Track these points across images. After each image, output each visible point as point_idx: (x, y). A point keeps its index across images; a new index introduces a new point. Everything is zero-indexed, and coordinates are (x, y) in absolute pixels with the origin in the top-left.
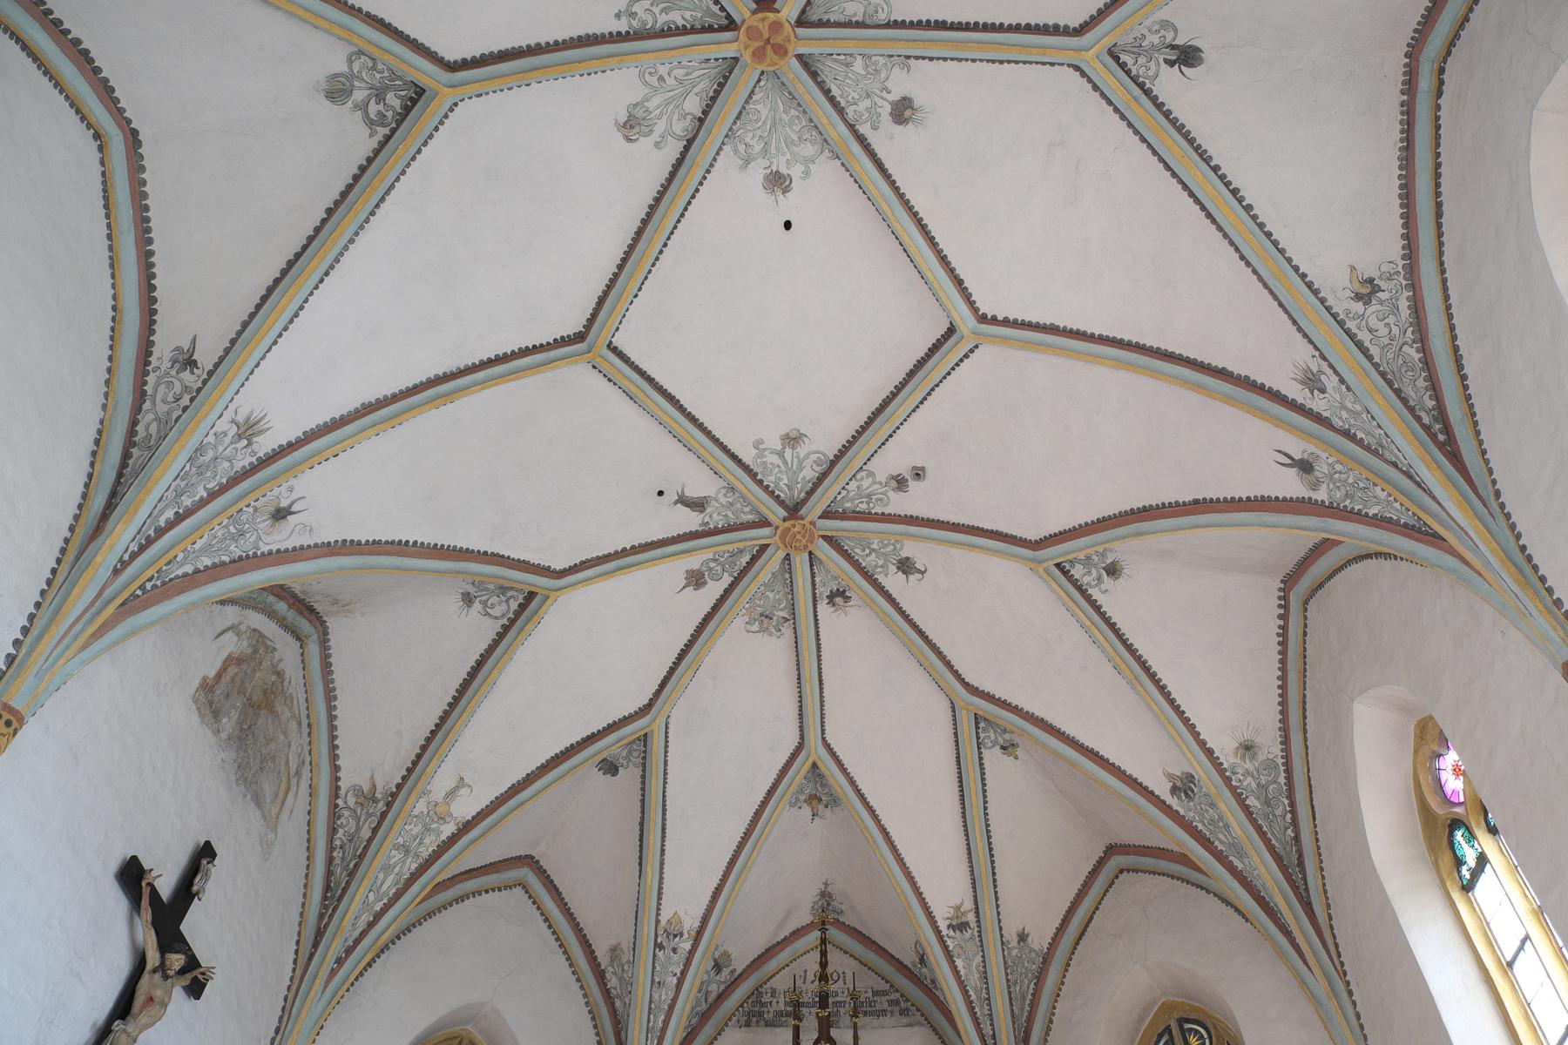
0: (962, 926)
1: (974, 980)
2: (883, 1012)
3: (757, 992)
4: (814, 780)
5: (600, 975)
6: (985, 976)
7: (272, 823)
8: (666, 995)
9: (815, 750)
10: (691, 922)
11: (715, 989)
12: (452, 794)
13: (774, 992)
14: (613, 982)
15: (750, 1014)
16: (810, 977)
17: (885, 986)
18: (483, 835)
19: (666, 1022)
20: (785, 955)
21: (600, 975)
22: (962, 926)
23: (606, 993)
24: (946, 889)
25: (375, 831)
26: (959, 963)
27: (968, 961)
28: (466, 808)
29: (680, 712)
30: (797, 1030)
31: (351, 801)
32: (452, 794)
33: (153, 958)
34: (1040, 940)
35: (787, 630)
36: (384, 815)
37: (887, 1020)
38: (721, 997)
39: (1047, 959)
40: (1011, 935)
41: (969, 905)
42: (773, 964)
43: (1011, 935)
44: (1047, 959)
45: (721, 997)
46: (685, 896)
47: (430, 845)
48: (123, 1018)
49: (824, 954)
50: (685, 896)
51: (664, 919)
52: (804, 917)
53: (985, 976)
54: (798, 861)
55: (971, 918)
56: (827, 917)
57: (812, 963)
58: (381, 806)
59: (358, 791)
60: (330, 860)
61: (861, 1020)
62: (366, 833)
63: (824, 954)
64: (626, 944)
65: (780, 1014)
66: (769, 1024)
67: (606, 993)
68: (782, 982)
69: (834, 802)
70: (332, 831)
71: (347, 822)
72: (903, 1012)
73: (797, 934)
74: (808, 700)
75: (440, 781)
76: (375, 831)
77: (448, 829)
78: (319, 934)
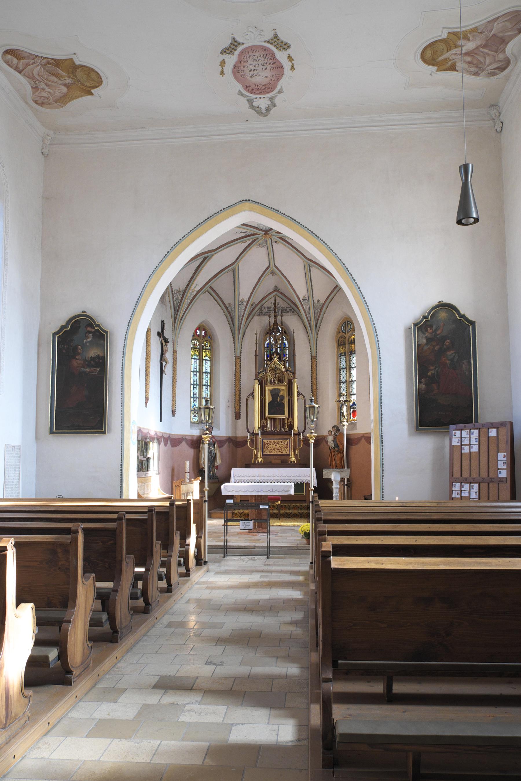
0: (305, 300)
1: (307, 310)
2: (288, 312)
3: (261, 308)
4: (272, 270)
5: (227, 308)
6: (309, 309)
7: (166, 306)
8: (242, 314)
10: (246, 299)
11: (251, 309)
12: (195, 287)
13: (264, 308)
14: (230, 310)
15: (259, 313)
16: (273, 304)
17: (289, 306)
18: (317, 641)
19: (242, 319)
20: (267, 299)
21: (227, 308)
22: (305, 300)
23: (229, 312)
24: (302, 292)
25: (182, 298)
26: (304, 307)
27: (306, 306)
28: (198, 289)
29: (241, 263)
30: (270, 317)
31: (176, 292)
32: (195, 287)
33: (164, 344)
34: (322, 301)
35: (266, 247)
37: (289, 314)
38: (253, 310)
39: (323, 304)
40: (316, 301)
41: (307, 296)
42: (264, 301)
43: (316, 301)
44: (323, 304)
45: (253, 310)
46: (244, 293)
48: (271, 463)
49: (275, 298)
50: (244, 293)
51: (240, 299)
52: (271, 291)
53: (309, 309)
54: (269, 284)
55: (307, 298)
56: (276, 289)
57: (273, 300)
59: (177, 290)
60: (174, 303)
61: (284, 314)
62: (180, 298)
63: (275, 298)
64: (232, 303)
65: (266, 312)
66: (263, 315)
67: (229, 312)
68: (266, 305)
70: (173, 298)
71: (176, 296)
72: (293, 312)
73: (269, 294)
74: (271, 260)
76: (182, 298)
77: (195, 293)
78: (175, 320)
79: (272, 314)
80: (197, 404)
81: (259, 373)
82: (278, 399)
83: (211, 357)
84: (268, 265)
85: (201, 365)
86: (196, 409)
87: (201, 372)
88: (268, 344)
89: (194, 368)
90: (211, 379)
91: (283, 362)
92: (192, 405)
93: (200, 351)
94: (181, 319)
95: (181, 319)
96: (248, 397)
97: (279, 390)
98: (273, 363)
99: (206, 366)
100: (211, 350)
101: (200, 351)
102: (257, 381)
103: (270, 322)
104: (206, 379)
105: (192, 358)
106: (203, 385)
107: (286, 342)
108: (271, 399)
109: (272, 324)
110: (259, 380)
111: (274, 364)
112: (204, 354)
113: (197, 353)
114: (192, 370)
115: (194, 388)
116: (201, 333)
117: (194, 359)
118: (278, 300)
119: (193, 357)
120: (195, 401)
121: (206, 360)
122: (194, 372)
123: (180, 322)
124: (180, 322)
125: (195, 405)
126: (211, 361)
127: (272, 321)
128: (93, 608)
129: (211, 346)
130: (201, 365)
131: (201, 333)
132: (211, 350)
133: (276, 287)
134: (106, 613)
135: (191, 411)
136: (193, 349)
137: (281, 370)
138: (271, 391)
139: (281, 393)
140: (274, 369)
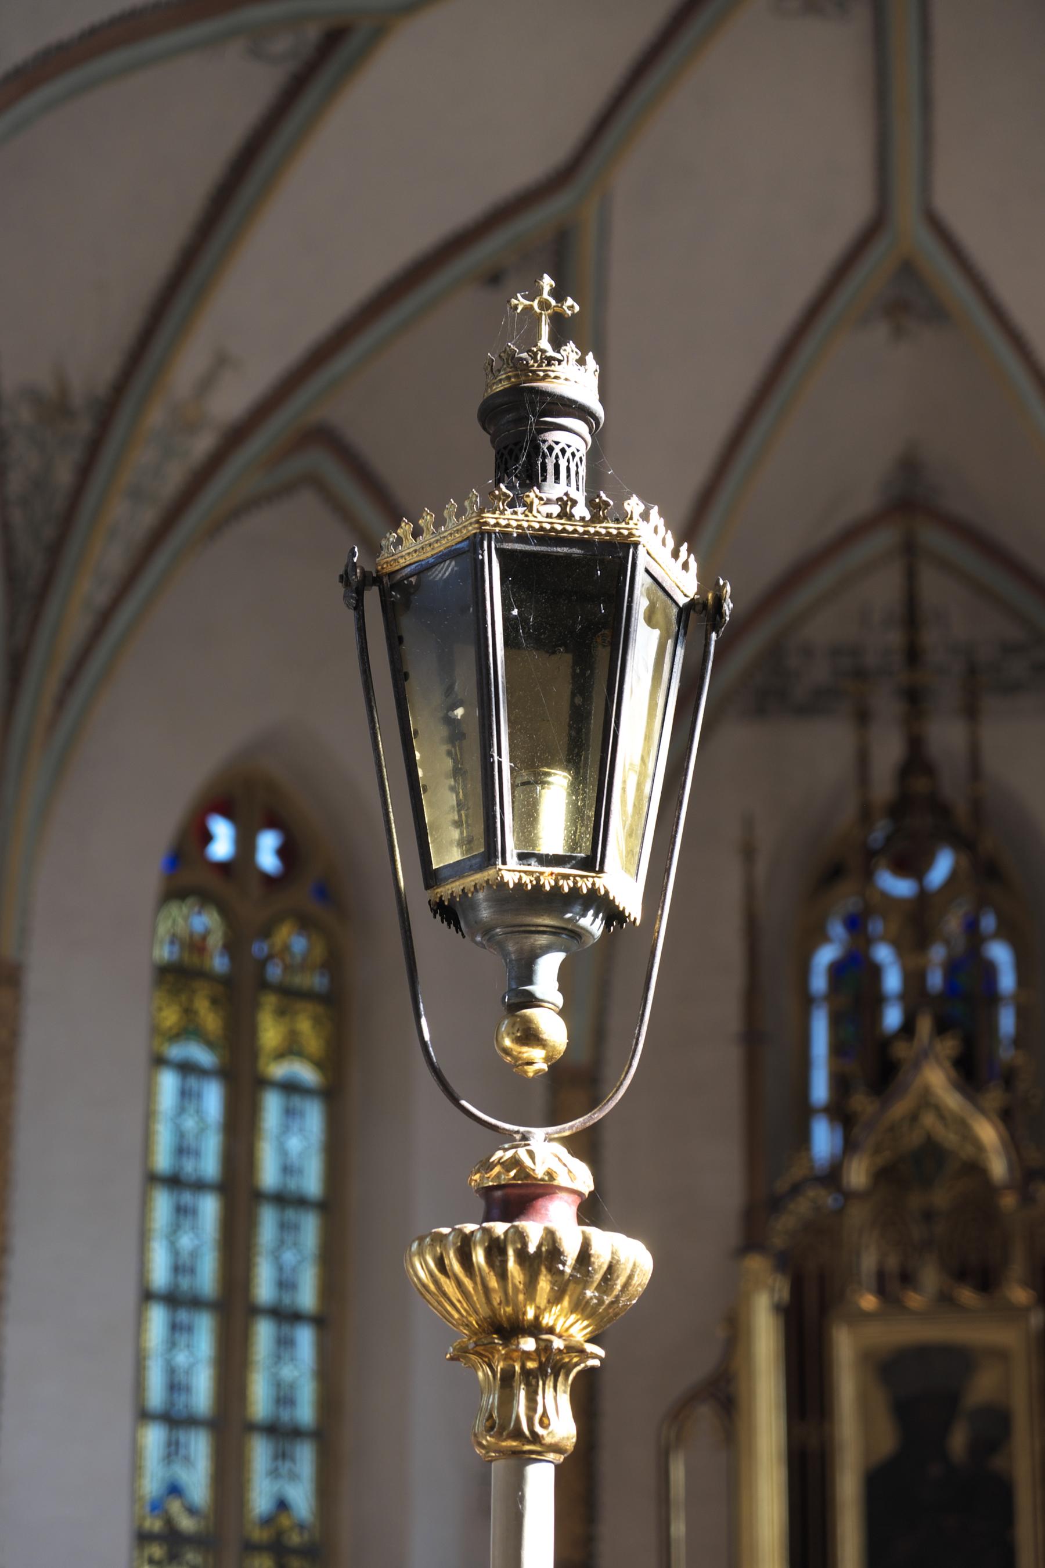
9: (908, 228)
12: (206, 384)
20: (826, 578)
25: (85, 471)
28: (231, 401)
29: (629, 175)
32: (206, 384)
36: (95, 447)
47: (174, 477)
52: (864, 501)
56: (910, 500)
57: (884, 590)
58: (84, 427)
62: (64, 475)
63: (911, 576)
69: (937, 313)
73: (852, 534)
75: (189, 365)
76: (85, 471)
77: (203, 444)
79: (887, 706)
80: (197, 1479)
81: (775, 1204)
82: (958, 1441)
83: (335, 1065)
84: (854, 208)
85: (240, 1129)
86: (186, 1524)
87: (238, 1190)
88: (836, 970)
89: (182, 1150)
90: (332, 1259)
91: (994, 1097)
92: (151, 1485)
93: (239, 995)
94: (70, 682)
95: (70, 682)
96: (679, 1413)
97: (961, 1360)
98: (900, 1108)
99: (291, 1145)
100: (335, 1004)
101: (239, 995)
102: (757, 1264)
103: (863, 759)
104: (287, 1262)
105: (159, 1061)
106: (254, 1311)
107: (1000, 954)
108: (887, 1443)
109: (883, 786)
110: (787, 1263)
111: (914, 1118)
112: (270, 1033)
113: (211, 1020)
114: (163, 1160)
115: (175, 1327)
116: (245, 845)
117: (186, 1068)
118: (935, 588)
119: (176, 1052)
120: (173, 1451)
121: (291, 1088)
122: (174, 1182)
123: (61, 703)
124: (61, 703)
125: (174, 1490)
126: (331, 1095)
127: (888, 751)
128: (513, 974)
129: (334, 964)
130: (240, 1129)
131: (245, 845)
132: (335, 1004)
133: (910, 466)
134: (568, 658)
135: (143, 1538)
136: (177, 976)
137: (976, 1169)
138: (889, 1369)
139: (983, 1387)
140: (916, 1167)
